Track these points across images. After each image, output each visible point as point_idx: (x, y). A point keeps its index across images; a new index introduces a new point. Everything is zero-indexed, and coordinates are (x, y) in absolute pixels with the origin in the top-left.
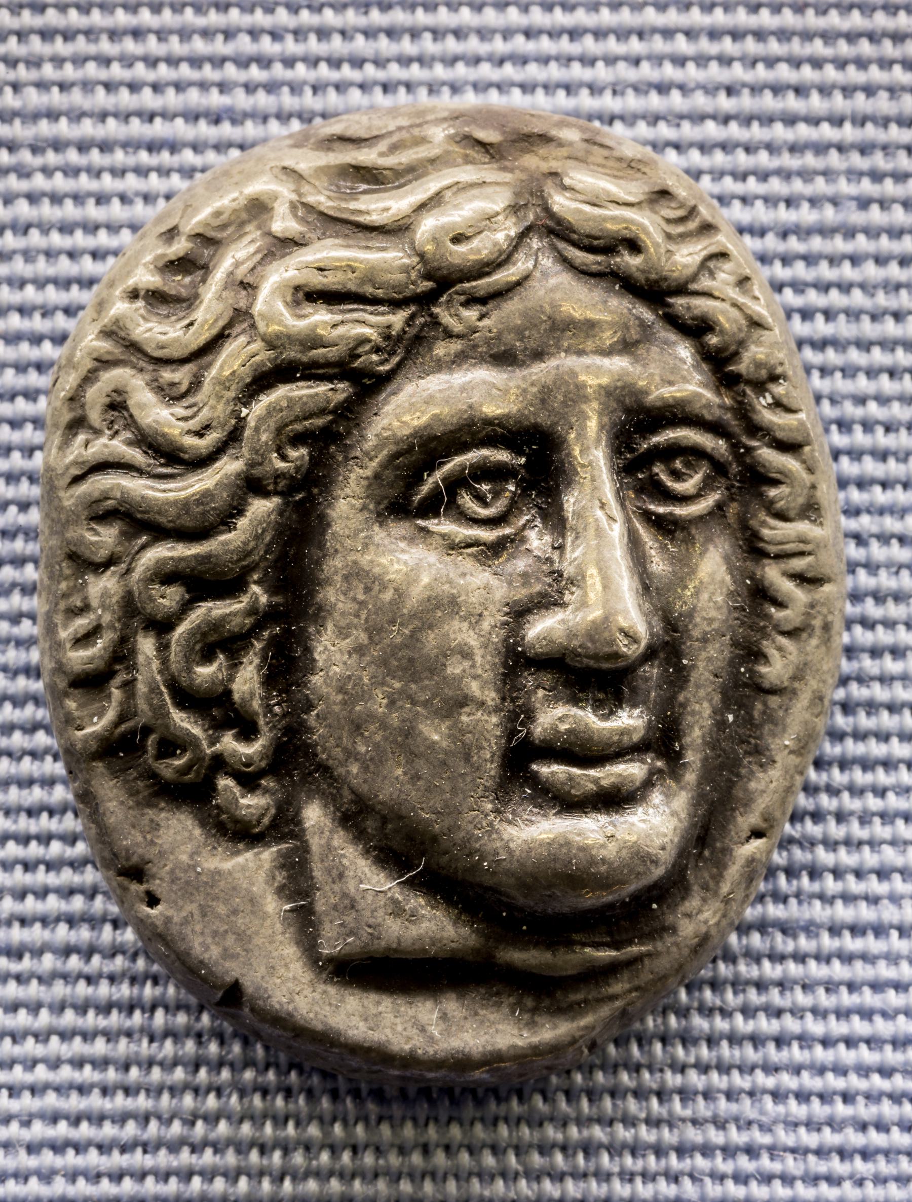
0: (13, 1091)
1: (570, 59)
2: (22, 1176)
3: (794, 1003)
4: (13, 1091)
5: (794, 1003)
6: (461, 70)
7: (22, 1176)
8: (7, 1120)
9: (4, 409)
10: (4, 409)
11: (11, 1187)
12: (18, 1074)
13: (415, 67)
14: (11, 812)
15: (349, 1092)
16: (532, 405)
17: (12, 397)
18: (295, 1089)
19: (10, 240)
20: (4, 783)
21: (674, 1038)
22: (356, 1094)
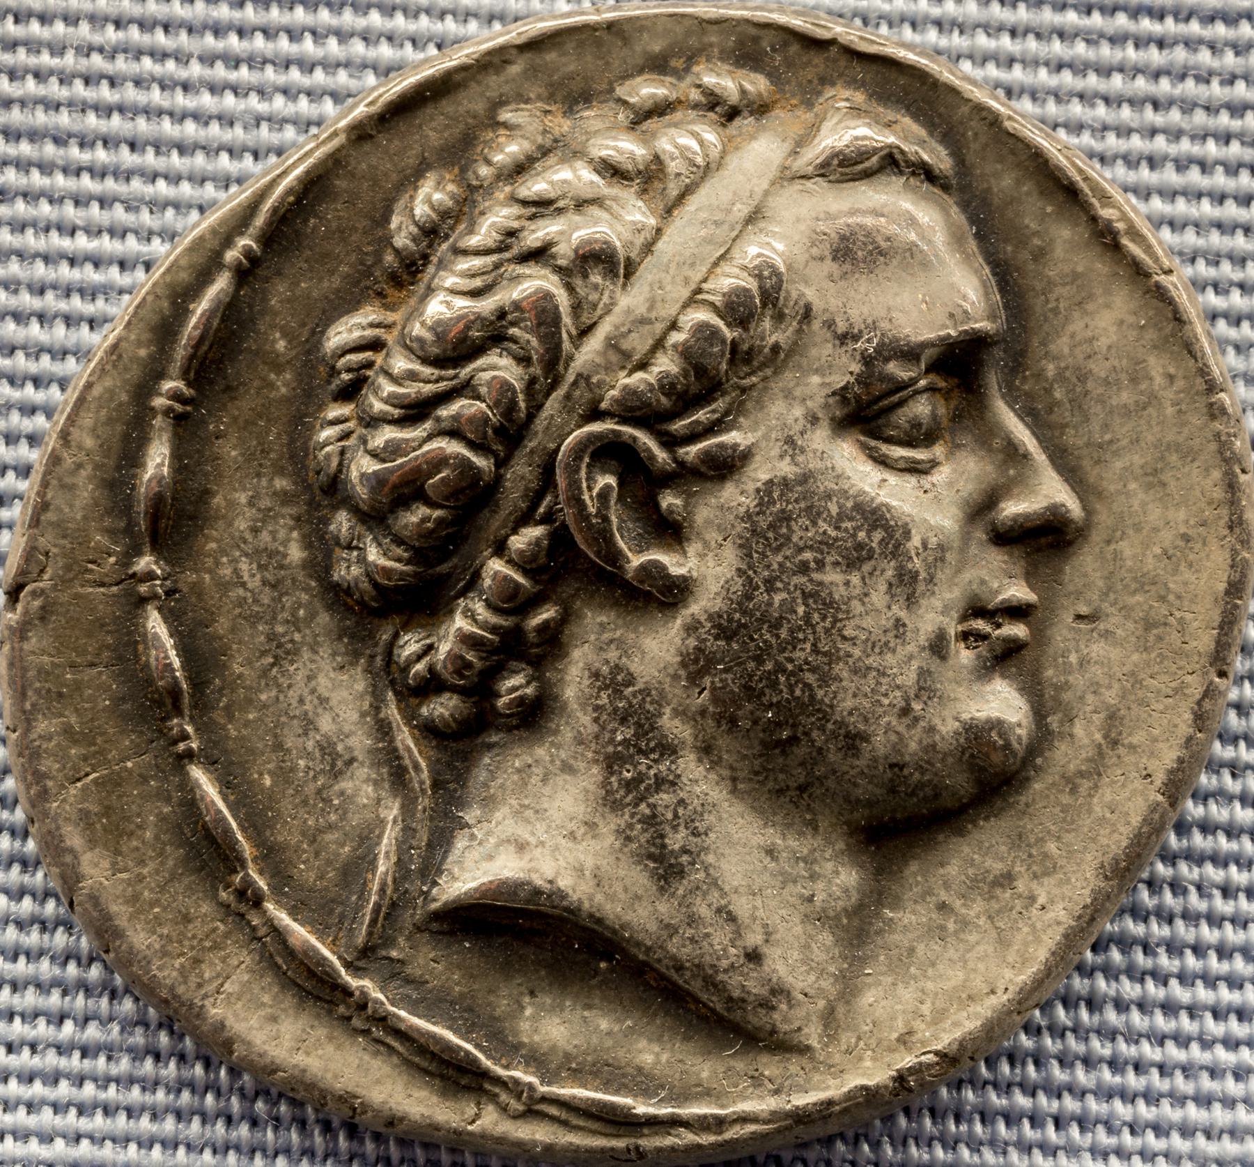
0: (13, 75)
1: (160, 113)
2: (22, 1135)
3: (1197, 938)
4: (13, 75)
5: (1197, 938)
6: (38, 1089)
7: (22, 1135)
8: (7, 103)
9: (7, 58)
10: (7, 58)
11: (9, 1146)
12: (21, 362)
13: (116, 119)
14: (10, 286)
15: (318, 1121)
16: (123, 699)
17: (12, 350)
18: (236, 1117)
19: (11, 176)
20: (8, 407)
21: (1158, 945)
22: (327, 1127)
